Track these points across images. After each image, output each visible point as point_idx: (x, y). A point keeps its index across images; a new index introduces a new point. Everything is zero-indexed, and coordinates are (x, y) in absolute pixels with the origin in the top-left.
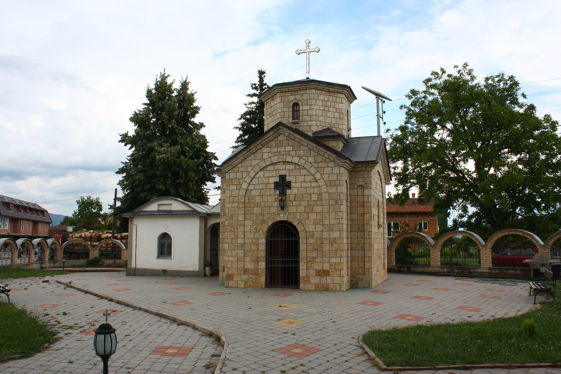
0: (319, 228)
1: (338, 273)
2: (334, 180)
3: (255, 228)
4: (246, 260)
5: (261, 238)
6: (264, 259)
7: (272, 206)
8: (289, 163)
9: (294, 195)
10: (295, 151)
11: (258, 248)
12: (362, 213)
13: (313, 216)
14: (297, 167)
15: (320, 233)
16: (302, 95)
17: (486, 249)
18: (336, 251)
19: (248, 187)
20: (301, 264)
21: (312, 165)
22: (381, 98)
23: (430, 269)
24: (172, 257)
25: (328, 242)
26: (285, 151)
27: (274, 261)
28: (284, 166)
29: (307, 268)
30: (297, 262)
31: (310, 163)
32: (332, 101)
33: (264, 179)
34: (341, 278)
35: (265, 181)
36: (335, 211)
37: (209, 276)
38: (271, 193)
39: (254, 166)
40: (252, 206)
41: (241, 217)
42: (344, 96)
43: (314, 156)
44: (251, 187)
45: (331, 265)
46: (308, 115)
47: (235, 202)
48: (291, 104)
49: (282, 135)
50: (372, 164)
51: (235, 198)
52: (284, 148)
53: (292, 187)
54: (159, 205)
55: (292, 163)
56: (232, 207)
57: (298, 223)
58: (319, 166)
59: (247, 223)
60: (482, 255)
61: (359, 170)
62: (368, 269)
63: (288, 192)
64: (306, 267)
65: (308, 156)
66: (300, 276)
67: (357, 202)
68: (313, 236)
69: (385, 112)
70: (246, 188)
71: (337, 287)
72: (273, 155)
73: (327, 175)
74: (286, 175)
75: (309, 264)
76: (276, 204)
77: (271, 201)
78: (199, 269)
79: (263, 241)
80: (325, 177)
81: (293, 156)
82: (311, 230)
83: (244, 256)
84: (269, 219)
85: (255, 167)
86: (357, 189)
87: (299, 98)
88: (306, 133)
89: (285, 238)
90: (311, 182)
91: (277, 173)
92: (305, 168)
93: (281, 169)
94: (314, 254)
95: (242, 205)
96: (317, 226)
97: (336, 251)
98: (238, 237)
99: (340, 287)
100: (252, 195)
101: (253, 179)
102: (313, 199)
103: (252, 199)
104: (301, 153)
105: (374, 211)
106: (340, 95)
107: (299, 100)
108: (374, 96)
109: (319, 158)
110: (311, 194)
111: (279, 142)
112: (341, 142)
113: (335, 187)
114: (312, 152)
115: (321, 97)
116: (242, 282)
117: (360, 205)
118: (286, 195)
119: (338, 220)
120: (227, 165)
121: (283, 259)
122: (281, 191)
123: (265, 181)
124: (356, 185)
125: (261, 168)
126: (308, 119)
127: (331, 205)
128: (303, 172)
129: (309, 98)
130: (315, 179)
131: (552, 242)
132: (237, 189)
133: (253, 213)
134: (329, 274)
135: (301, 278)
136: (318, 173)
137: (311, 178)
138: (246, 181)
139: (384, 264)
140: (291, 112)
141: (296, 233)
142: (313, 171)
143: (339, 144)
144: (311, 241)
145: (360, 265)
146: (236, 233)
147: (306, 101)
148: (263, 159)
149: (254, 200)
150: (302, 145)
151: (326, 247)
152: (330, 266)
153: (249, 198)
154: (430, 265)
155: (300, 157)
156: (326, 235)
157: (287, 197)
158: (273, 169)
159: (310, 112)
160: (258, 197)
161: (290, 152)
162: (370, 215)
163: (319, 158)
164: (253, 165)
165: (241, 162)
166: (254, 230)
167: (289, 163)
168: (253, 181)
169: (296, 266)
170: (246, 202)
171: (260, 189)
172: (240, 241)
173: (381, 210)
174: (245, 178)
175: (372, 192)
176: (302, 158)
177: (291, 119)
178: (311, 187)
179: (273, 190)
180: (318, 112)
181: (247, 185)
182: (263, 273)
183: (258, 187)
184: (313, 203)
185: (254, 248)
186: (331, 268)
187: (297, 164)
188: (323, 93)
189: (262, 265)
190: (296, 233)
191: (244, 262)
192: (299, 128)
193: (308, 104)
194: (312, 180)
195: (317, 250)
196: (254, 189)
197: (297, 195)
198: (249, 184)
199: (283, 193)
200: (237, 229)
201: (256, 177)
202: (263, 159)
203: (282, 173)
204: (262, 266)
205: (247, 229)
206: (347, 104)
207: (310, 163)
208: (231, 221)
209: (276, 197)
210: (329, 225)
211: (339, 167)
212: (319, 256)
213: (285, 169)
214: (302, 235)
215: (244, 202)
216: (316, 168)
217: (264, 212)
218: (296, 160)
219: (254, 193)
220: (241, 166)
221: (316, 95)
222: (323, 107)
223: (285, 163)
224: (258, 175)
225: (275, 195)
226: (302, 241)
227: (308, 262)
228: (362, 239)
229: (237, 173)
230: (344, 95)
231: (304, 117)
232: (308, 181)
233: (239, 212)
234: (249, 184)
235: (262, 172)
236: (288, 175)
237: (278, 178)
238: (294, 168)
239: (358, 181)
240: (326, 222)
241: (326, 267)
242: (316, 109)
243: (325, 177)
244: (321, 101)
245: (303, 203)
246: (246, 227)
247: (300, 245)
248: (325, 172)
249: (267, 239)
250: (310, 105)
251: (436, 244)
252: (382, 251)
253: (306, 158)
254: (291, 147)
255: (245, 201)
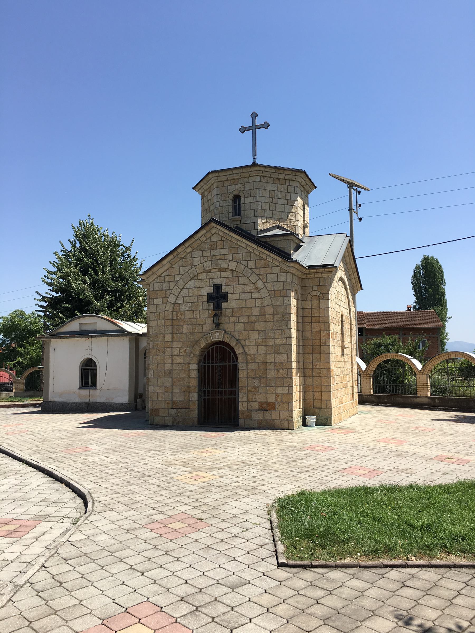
0: (262, 349)
1: (286, 406)
2: (280, 289)
3: (185, 351)
4: (175, 391)
5: (192, 364)
6: (196, 389)
7: (205, 324)
8: (225, 270)
9: (231, 310)
10: (232, 254)
11: (189, 376)
12: (317, 330)
13: (254, 335)
14: (235, 274)
15: (263, 356)
16: (244, 184)
17: (423, 375)
18: (283, 378)
19: (176, 301)
20: (240, 395)
21: (253, 272)
22: (355, 188)
23: (418, 400)
24: (97, 388)
25: (273, 368)
26: (220, 255)
27: (209, 392)
28: (219, 273)
29: (248, 399)
30: (236, 393)
31: (250, 269)
32: (282, 190)
33: (195, 290)
34: (289, 413)
35: (196, 293)
36: (281, 328)
37: (141, 409)
38: (204, 308)
39: (183, 275)
40: (182, 324)
41: (168, 338)
42: (298, 184)
43: (255, 260)
44: (180, 301)
45: (277, 396)
46: (251, 209)
47: (161, 319)
48: (231, 197)
49: (215, 235)
50: (329, 268)
51: (161, 314)
52: (218, 250)
53: (228, 299)
54: (81, 324)
55: (228, 270)
56: (157, 326)
57: (237, 344)
58: (261, 273)
59: (175, 344)
60: (363, 381)
61: (314, 277)
62: (326, 401)
63: (224, 305)
64: (246, 399)
65: (247, 261)
66: (239, 410)
67: (311, 316)
68: (254, 360)
69: (360, 205)
70: (173, 301)
71: (285, 424)
72: (206, 260)
73: (272, 283)
74: (221, 285)
75: (250, 394)
76: (210, 321)
77: (204, 317)
78: (129, 401)
79: (194, 366)
80: (269, 286)
81: (229, 260)
82: (252, 352)
83: (172, 386)
84: (202, 340)
85: (185, 275)
86: (311, 300)
87: (240, 187)
88: (249, 232)
89: (221, 363)
90: (252, 292)
91: (211, 282)
92: (245, 276)
93: (216, 277)
94: (257, 384)
95: (168, 323)
96: (260, 347)
97: (283, 378)
98: (165, 361)
99: (289, 424)
100: (181, 310)
101: (181, 290)
102: (254, 314)
103: (181, 315)
104: (240, 256)
105: (334, 328)
106: (292, 183)
107: (240, 191)
108: (346, 185)
109: (261, 263)
110: (252, 307)
111: (213, 243)
112: (292, 242)
113: (281, 299)
114: (252, 254)
115: (269, 187)
116: (169, 418)
117: (316, 320)
118: (222, 310)
119: (285, 340)
120: (150, 273)
121: (206, 389)
122: (215, 304)
123: (197, 292)
124: (309, 295)
125: (192, 277)
126: (252, 215)
127: (277, 321)
128: (243, 280)
129: (252, 188)
130: (257, 288)
131: (394, 358)
132: (163, 303)
133: (182, 333)
134: (275, 408)
135: (240, 412)
136: (260, 281)
137: (251, 288)
138: (173, 293)
139: (353, 394)
140: (231, 206)
141: (234, 357)
142: (253, 278)
143: (290, 244)
144: (253, 366)
145: (316, 396)
146: (162, 358)
147: (249, 191)
148: (193, 265)
149: (183, 317)
150: (241, 246)
151: (271, 374)
152: (276, 398)
153: (177, 314)
154: (417, 394)
155: (238, 262)
156: (270, 359)
157: (223, 311)
158: (206, 278)
159: (254, 206)
160: (189, 312)
161: (226, 256)
162: (327, 332)
163: (261, 263)
164: (182, 273)
165: (168, 269)
166: (183, 353)
167: (225, 270)
168: (182, 291)
169: (235, 397)
170: (174, 318)
171: (191, 303)
172: (167, 367)
173: (347, 326)
174: (172, 289)
175: (332, 304)
176: (240, 263)
177: (231, 214)
178: (252, 299)
179: (206, 304)
180: (263, 205)
181: (175, 299)
182: (195, 406)
183: (188, 299)
184: (254, 319)
185: (183, 375)
186: (276, 400)
187: (235, 270)
188: (271, 180)
189: (194, 396)
190: (234, 357)
191: (172, 392)
192: (241, 226)
193: (252, 195)
194: (253, 290)
195: (260, 377)
196: (184, 303)
197: (235, 309)
198: (177, 297)
199: (218, 307)
200: (164, 352)
201: (185, 287)
202: (193, 265)
203: (217, 282)
204: (193, 398)
205: (176, 352)
206: (303, 194)
207: (250, 269)
208: (157, 343)
209: (210, 312)
210: (274, 346)
211: (286, 273)
212: (262, 385)
213: (221, 278)
214: (240, 358)
215: (172, 319)
216: (257, 275)
217: (196, 331)
218: (233, 265)
219: (183, 308)
220: (167, 274)
221: (262, 184)
222: (271, 199)
223: (221, 270)
224: (188, 286)
225: (209, 310)
226: (241, 366)
227: (249, 392)
228: (318, 363)
229: (163, 283)
230: (298, 183)
231: (246, 212)
232: (248, 291)
233: (167, 332)
234: (177, 297)
235: (193, 281)
236: (223, 284)
237: (212, 288)
238: (231, 275)
239: (312, 290)
240: (271, 342)
241: (272, 399)
242: (261, 202)
243: (269, 286)
244: (268, 191)
245: (243, 320)
246: (174, 350)
247: (239, 371)
248: (268, 279)
249: (199, 364)
250: (254, 197)
251: (424, 368)
252: (349, 378)
253: (245, 263)
254: (227, 250)
255: (172, 317)
